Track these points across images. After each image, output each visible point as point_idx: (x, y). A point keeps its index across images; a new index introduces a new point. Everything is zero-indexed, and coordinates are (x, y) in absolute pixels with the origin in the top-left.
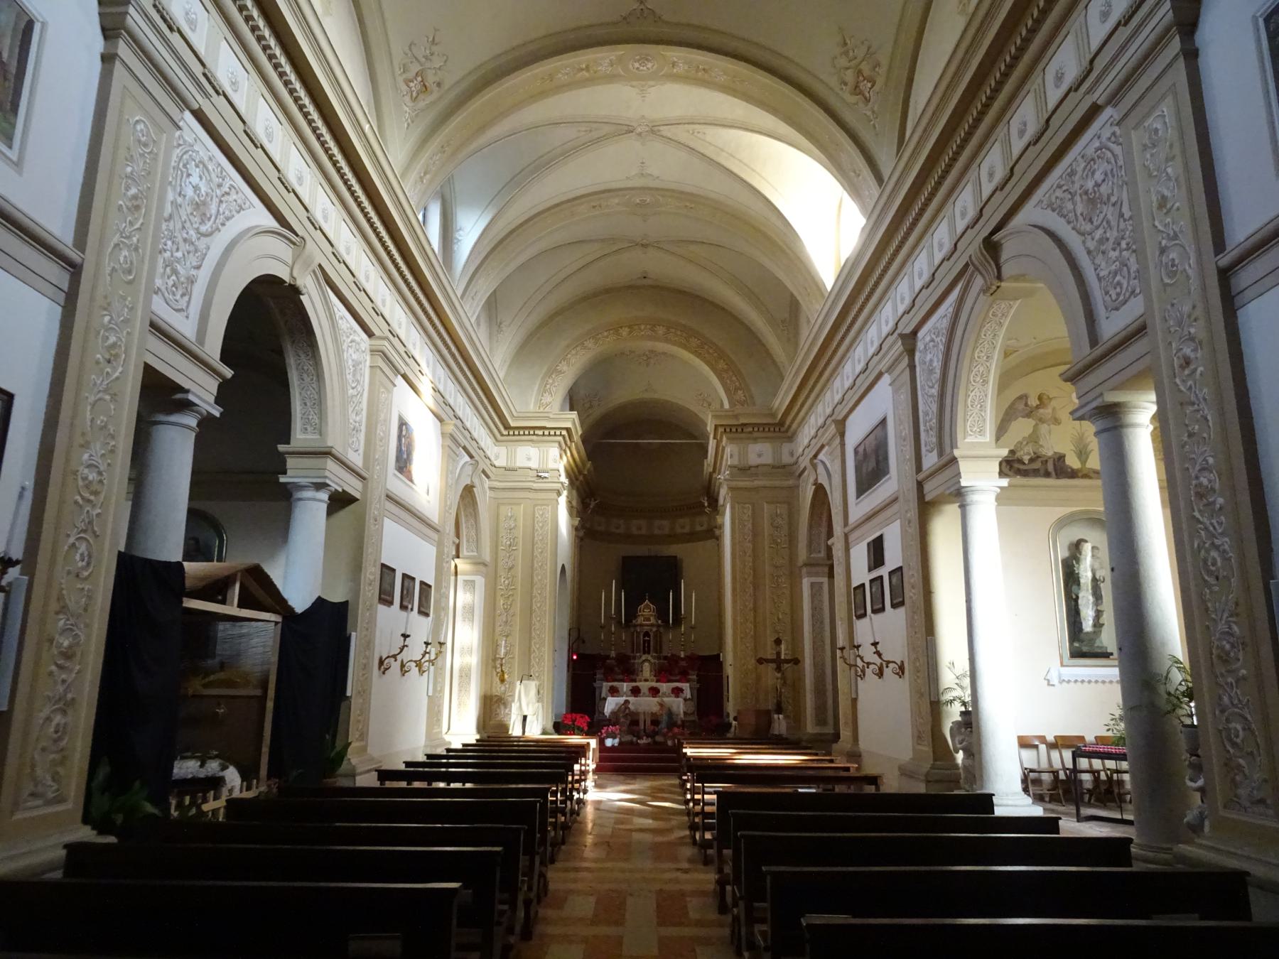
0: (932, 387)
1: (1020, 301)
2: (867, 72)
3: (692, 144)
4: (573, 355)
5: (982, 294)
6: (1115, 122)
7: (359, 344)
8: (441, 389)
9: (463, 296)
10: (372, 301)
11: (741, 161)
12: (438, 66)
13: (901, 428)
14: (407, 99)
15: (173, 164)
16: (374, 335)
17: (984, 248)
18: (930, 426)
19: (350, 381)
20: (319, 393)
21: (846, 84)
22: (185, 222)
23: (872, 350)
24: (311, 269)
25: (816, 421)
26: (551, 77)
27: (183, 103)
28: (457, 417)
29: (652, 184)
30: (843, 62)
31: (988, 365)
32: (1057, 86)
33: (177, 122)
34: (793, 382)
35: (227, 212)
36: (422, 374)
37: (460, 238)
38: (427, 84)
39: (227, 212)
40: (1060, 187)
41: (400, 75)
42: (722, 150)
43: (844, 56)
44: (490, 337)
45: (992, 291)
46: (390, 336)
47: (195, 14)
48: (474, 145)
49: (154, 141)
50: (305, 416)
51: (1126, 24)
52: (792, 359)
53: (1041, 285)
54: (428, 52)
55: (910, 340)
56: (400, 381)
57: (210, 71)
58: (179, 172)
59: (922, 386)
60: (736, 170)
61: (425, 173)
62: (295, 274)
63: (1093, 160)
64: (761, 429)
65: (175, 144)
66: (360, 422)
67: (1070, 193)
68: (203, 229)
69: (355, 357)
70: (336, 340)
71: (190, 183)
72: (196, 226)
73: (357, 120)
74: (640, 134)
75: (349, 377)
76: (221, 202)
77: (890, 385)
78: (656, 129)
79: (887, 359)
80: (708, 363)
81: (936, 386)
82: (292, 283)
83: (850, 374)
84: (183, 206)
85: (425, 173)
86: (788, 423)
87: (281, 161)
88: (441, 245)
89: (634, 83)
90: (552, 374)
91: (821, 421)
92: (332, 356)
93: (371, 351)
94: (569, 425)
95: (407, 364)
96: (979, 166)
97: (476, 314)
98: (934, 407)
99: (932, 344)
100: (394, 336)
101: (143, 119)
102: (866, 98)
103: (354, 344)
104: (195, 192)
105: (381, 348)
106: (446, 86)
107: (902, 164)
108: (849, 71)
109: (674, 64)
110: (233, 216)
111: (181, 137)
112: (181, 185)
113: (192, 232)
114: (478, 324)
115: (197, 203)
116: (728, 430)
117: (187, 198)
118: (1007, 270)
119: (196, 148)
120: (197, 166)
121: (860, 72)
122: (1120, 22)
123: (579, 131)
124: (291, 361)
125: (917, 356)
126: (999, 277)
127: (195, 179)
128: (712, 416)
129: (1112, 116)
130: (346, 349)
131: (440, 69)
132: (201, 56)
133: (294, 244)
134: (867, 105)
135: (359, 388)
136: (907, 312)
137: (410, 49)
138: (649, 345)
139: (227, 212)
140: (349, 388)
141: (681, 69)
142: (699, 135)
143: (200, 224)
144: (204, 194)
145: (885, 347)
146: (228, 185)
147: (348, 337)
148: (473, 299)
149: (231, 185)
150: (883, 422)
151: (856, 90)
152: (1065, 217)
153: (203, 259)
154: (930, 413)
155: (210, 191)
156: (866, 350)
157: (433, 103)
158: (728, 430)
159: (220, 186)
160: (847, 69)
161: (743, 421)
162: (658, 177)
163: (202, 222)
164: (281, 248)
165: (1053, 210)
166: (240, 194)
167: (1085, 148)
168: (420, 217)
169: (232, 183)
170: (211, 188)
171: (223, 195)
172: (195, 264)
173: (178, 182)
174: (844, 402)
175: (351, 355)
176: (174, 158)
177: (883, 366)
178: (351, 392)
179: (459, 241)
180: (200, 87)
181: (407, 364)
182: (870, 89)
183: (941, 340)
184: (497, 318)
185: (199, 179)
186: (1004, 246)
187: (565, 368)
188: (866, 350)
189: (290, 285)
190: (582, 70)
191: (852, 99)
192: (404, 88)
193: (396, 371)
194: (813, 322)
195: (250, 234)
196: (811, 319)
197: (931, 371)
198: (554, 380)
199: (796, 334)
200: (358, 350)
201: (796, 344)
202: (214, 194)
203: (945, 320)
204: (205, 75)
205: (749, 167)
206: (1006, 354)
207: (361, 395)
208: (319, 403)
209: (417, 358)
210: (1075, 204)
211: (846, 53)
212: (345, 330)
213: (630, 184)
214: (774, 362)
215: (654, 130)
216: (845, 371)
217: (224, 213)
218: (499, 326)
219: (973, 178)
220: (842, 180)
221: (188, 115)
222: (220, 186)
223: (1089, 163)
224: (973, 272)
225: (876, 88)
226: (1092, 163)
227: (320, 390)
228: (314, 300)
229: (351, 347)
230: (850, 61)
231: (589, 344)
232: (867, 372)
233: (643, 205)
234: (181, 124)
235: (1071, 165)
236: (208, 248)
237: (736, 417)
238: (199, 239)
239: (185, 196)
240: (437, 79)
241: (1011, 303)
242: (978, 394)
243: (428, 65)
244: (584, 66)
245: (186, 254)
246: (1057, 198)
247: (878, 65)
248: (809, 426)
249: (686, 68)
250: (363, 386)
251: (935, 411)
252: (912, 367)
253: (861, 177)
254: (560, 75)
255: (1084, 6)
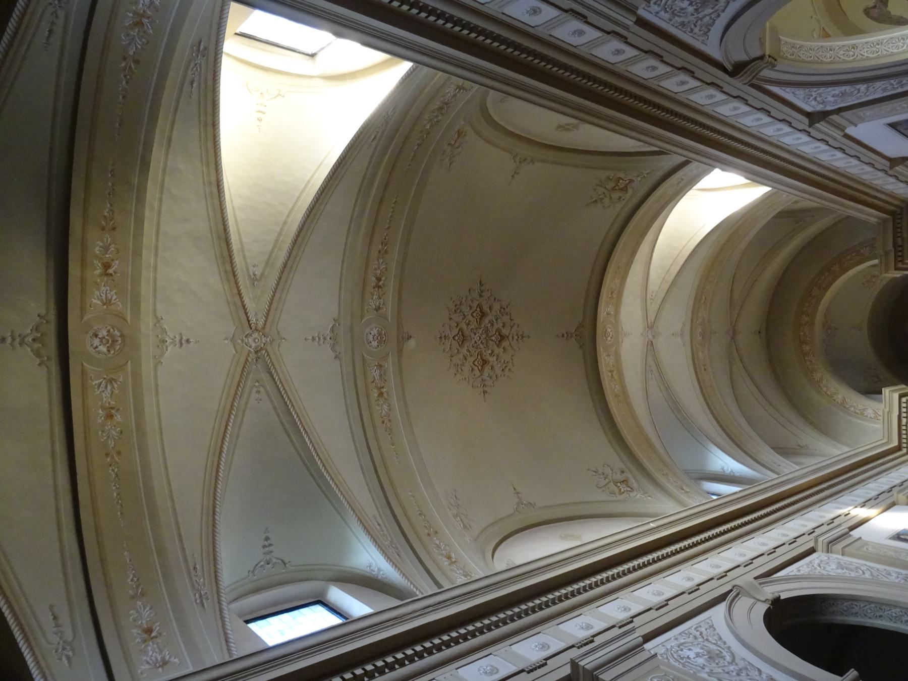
0: (859, 90)
1: (780, 37)
2: (612, 184)
3: (660, 300)
4: (828, 390)
5: (775, 68)
6: (648, 4)
7: (821, 561)
8: (864, 500)
9: (778, 474)
10: (784, 544)
11: (671, 265)
12: (611, 472)
13: (898, 108)
14: (632, 494)
15: (681, 666)
16: (813, 548)
17: (737, 75)
18: (897, 84)
19: (857, 574)
20: (871, 603)
21: (620, 197)
22: (723, 670)
23: (824, 147)
24: (758, 586)
25: (867, 173)
26: (616, 396)
27: (636, 648)
28: (890, 490)
29: (688, 327)
30: (606, 201)
31: (838, 48)
32: (740, 108)
33: (651, 655)
34: (849, 207)
35: (715, 638)
36: (849, 514)
37: (730, 470)
38: (622, 480)
39: (715, 637)
40: (692, 30)
41: (616, 497)
42: (664, 278)
43: (603, 201)
44: (812, 455)
45: (773, 61)
46: (814, 534)
47: (582, 623)
48: (661, 451)
49: (665, 675)
50: (893, 619)
51: (585, 17)
52: (831, 211)
53: (768, 24)
54: (602, 476)
55: (814, 118)
56: (855, 533)
57: (617, 623)
58: (687, 664)
59: (858, 98)
60: (678, 268)
61: (683, 489)
62: (763, 599)
63: (673, 12)
64: (899, 230)
65: (666, 661)
66: (898, 574)
67: (696, 22)
68: (728, 658)
69: (834, 567)
70: (822, 578)
71: (694, 658)
72: (726, 664)
73: (647, 531)
74: (654, 337)
75: (853, 574)
76: (707, 640)
77: (856, 126)
78: (650, 326)
79: (831, 132)
80: (834, 280)
81: (858, 87)
82: (770, 602)
83: (846, 161)
84: (712, 668)
85: (683, 489)
86: (892, 208)
87: (676, 590)
88: (737, 485)
89: (620, 340)
90: (845, 408)
91: (892, 180)
92: (859, 587)
93: (828, 552)
94: (896, 396)
95: (840, 525)
96: (676, 93)
97: (792, 464)
98: (878, 84)
99: (818, 99)
100: (814, 532)
101: (650, 678)
102: (629, 182)
103: (821, 565)
104: (700, 657)
105: (825, 545)
106: (623, 466)
107: (699, 158)
108: (612, 196)
109: (608, 314)
110: (718, 634)
111: (661, 655)
112: (696, 666)
113: (732, 668)
114: (801, 464)
115: (709, 657)
116: (900, 259)
117: (706, 664)
118: (758, 53)
119: (669, 647)
120: (682, 650)
121: (613, 189)
122: (768, 115)
123: (652, 379)
124: (840, 619)
125: (829, 108)
126: (761, 58)
127: (692, 654)
128: (886, 273)
129: (644, 8)
130: (827, 572)
131: (612, 470)
132: (609, 626)
133: (738, 594)
134: (634, 181)
135: (864, 568)
136: (790, 124)
137: (601, 488)
138: (818, 327)
139: (715, 637)
140: (863, 576)
141: (611, 309)
142: (654, 296)
143: (725, 660)
144: (701, 651)
145: (781, 117)
146: (695, 632)
147: (816, 568)
148: (779, 465)
149: (695, 629)
150: (893, 126)
151: (624, 190)
152: (715, 20)
153: (753, 665)
154: (883, 87)
155: (699, 646)
156: (823, 151)
157: (635, 478)
158: (900, 259)
159: (695, 638)
160: (611, 198)
161: (890, 246)
162: (683, 324)
163: (723, 658)
164: (743, 604)
165: (709, 30)
166: (701, 624)
167: (664, 20)
168: (715, 497)
169: (693, 628)
170: (698, 644)
171: (703, 637)
172: (757, 673)
173: (694, 667)
174: (858, 155)
175: (832, 569)
176: (676, 664)
177: (837, 134)
178: (867, 575)
179: (732, 471)
180: (628, 633)
181: (840, 525)
182: (623, 180)
183: (815, 92)
184: (795, 449)
185: (691, 651)
186: (736, 60)
187: (840, 396)
188: (823, 151)
189: (771, 605)
190: (612, 375)
191: (630, 191)
192: (625, 495)
193: (845, 535)
194: (798, 198)
195: (732, 625)
196: (794, 200)
197: (843, 94)
198: (852, 406)
199: (808, 210)
200: (828, 563)
201: (818, 209)
202: (702, 643)
203: (797, 92)
204: (620, 627)
205: (676, 259)
206: (827, 36)
207: (871, 567)
208: (881, 605)
209: (833, 516)
210: (705, 16)
211: (601, 199)
212: (810, 569)
213: (688, 343)
214: (835, 224)
215: (651, 327)
216: (843, 166)
217: (716, 640)
218: (802, 447)
219: (655, 82)
220: (684, 192)
221: (647, 646)
222: (695, 638)
223: (676, 15)
224: (758, 79)
225: (622, 176)
226: (675, 12)
227: (867, 601)
228: (787, 591)
229: (825, 568)
230: (606, 196)
231: (817, 376)
232: (843, 147)
233: (703, 334)
234: (653, 653)
235: (676, 27)
236: (744, 659)
237: (887, 253)
238: (737, 664)
239: (704, 665)
240: (619, 473)
241: (782, 43)
242: (865, 50)
243: (610, 477)
244: (610, 374)
245: (749, 677)
246: (700, 31)
247: (608, 178)
248: (875, 179)
249: (610, 306)
250: (862, 565)
251: (882, 83)
252: (839, 111)
253: (683, 177)
254: (616, 390)
255: (482, 6)
